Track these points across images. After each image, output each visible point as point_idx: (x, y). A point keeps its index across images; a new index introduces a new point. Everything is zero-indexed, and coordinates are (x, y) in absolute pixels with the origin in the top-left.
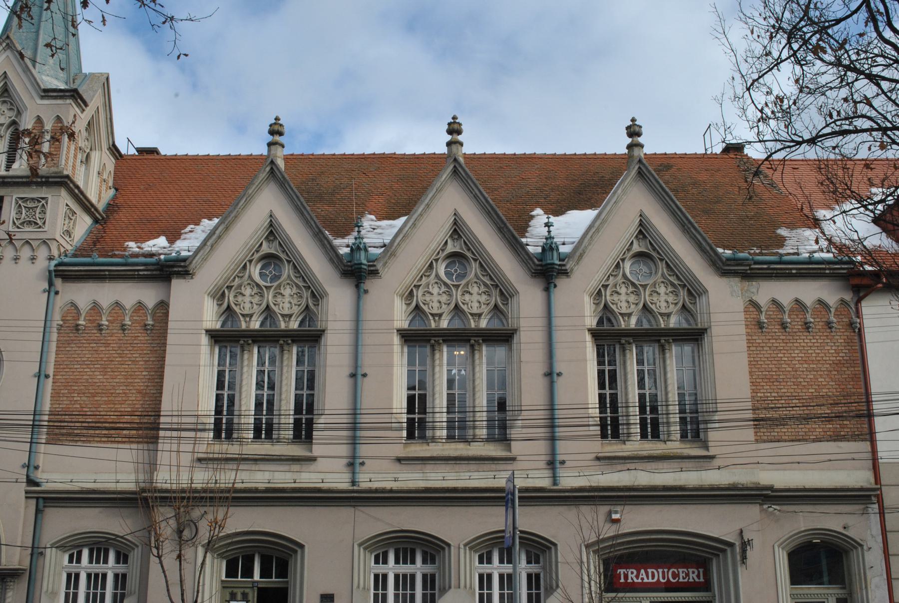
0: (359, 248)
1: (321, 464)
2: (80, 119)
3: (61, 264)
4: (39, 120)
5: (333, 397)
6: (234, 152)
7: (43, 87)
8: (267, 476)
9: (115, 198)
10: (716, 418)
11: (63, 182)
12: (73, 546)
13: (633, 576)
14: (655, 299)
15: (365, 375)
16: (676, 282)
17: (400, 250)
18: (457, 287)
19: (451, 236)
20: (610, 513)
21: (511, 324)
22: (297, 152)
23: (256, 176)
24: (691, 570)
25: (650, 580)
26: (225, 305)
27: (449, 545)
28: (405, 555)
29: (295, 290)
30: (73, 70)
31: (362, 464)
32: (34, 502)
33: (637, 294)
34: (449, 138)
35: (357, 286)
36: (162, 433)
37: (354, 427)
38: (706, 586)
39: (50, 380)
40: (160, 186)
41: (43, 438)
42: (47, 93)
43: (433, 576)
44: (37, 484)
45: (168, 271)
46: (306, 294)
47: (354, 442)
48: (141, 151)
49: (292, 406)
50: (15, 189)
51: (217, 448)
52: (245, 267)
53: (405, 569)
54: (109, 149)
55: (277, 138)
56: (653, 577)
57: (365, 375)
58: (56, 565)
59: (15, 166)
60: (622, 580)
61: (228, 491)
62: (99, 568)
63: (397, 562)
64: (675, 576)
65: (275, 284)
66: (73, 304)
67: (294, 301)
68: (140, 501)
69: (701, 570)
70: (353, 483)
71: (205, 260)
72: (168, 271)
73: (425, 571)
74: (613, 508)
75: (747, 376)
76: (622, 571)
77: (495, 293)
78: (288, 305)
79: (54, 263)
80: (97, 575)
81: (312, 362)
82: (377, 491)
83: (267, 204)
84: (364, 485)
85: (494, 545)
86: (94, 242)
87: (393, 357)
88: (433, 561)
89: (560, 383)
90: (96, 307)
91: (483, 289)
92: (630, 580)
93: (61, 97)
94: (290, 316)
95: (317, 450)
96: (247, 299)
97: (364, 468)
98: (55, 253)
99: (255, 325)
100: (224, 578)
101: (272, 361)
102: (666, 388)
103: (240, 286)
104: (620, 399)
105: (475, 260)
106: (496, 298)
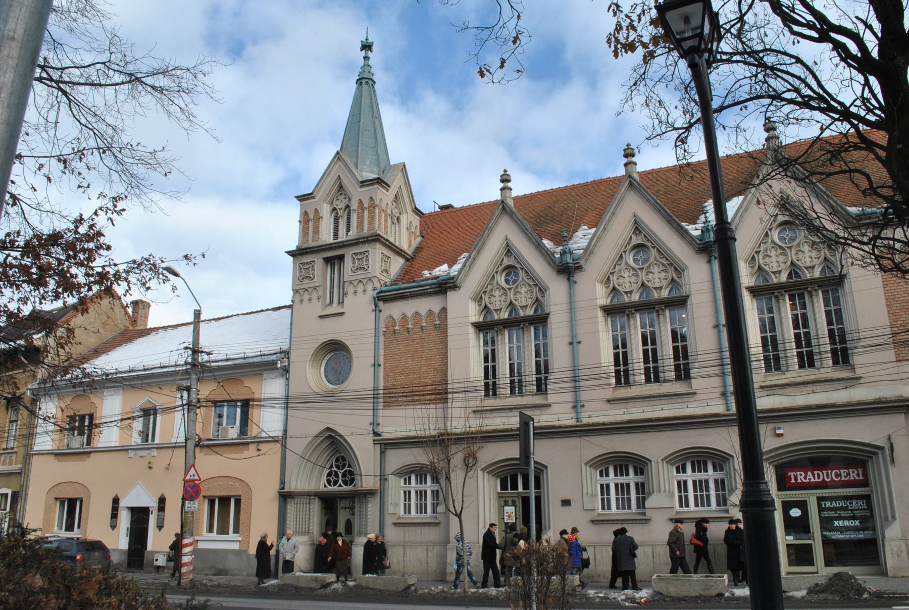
0: (565, 252)
1: (555, 408)
2: (384, 197)
3: (381, 292)
4: (361, 202)
5: (559, 359)
6: (548, 188)
7: (361, 180)
8: (504, 420)
9: (421, 242)
10: (860, 344)
11: (375, 239)
12: (405, 473)
13: (802, 477)
14: (800, 256)
15: (579, 342)
16: (665, 263)
17: (596, 249)
18: (790, 248)
19: (634, 232)
20: (775, 429)
21: (684, 291)
22: (521, 194)
23: (493, 214)
24: (851, 471)
25: (817, 480)
26: (483, 305)
27: (650, 461)
28: (621, 470)
29: (528, 288)
30: (383, 165)
31: (583, 406)
32: (378, 446)
33: (785, 255)
34: (502, 185)
35: (568, 279)
36: (450, 396)
37: (575, 379)
38: (865, 483)
39: (382, 367)
40: (454, 229)
41: (381, 406)
42: (364, 183)
43: (723, 481)
44: (379, 435)
45: (444, 287)
46: (535, 290)
47: (576, 390)
48: (441, 208)
49: (534, 369)
50: (350, 248)
51: (804, 372)
52: (493, 277)
53: (701, 476)
54: (413, 211)
55: (772, 132)
56: (819, 477)
57: (579, 342)
58: (396, 487)
59: (350, 234)
60: (793, 481)
61: (477, 432)
62: (701, 476)
63: (616, 475)
64: (837, 475)
65: (646, 265)
66: (391, 317)
67: (528, 296)
68: (442, 441)
69: (860, 470)
70: (578, 419)
71: (466, 276)
72: (444, 287)
73: (637, 481)
74: (777, 425)
75: (885, 309)
76: (792, 474)
77: (671, 270)
78: (524, 299)
79: (376, 292)
80: (421, 492)
81: (837, 302)
82: (593, 425)
83: (504, 231)
84: (585, 421)
85: (686, 459)
86: (406, 274)
87: (598, 325)
88: (721, 469)
89: (582, 348)
90: (404, 317)
91: (662, 268)
92: (799, 481)
93: (372, 184)
94: (661, 288)
95: (551, 398)
96: (497, 299)
97: (583, 409)
98: (378, 285)
99: (636, 297)
100: (499, 490)
101: (622, 328)
102: (816, 326)
103: (491, 290)
104: (779, 338)
105: (654, 247)
106: (672, 274)
